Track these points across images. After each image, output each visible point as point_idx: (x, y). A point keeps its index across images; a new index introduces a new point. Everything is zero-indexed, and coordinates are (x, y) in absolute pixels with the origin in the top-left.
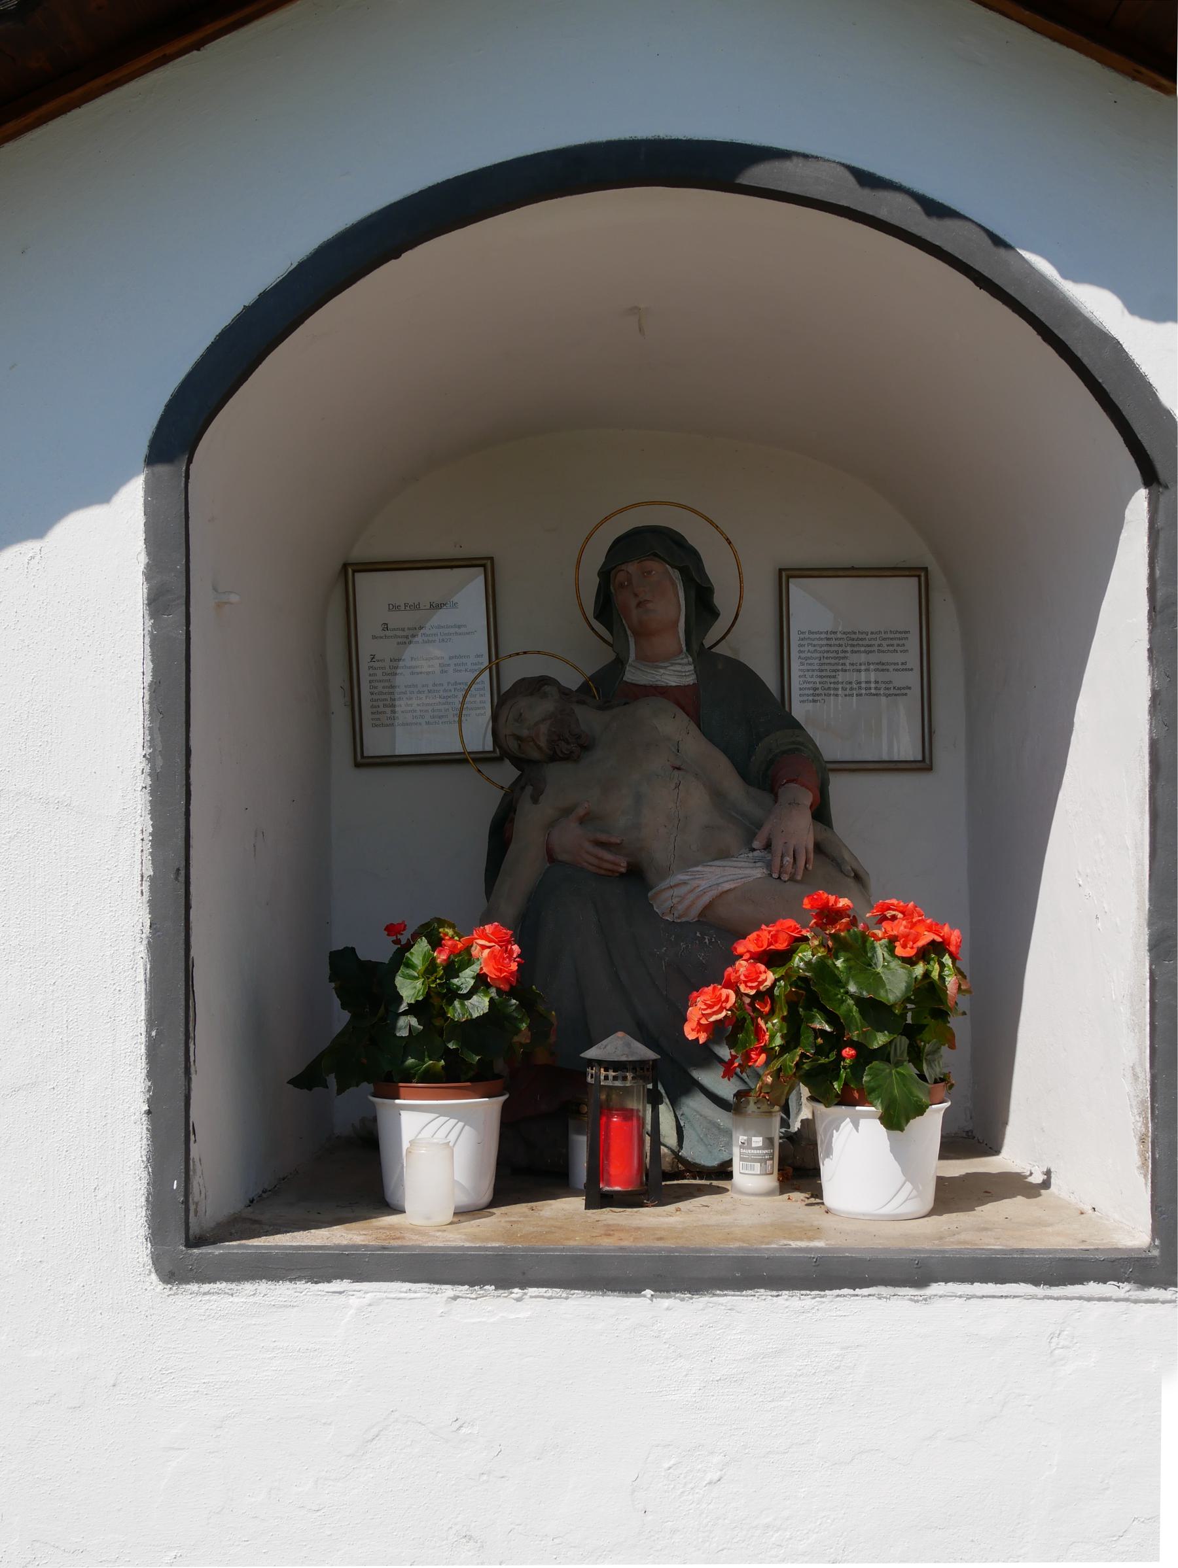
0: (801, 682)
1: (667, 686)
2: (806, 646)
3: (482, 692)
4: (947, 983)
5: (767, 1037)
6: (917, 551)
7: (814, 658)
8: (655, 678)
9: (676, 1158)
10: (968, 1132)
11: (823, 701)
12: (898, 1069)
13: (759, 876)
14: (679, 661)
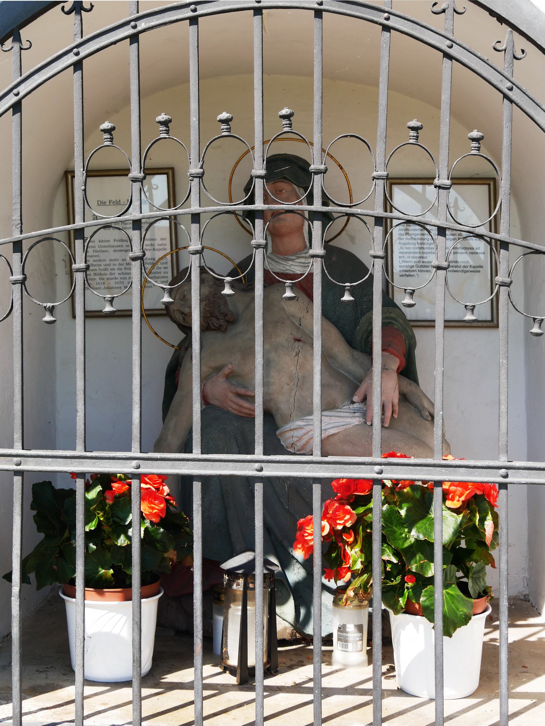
0: (401, 262)
1: (294, 274)
2: (404, 239)
3: (166, 266)
4: (485, 526)
5: (351, 561)
6: (485, 169)
7: (410, 244)
8: (285, 268)
9: (294, 629)
10: (525, 595)
11: (417, 275)
12: (447, 590)
13: (357, 423)
14: (303, 255)
